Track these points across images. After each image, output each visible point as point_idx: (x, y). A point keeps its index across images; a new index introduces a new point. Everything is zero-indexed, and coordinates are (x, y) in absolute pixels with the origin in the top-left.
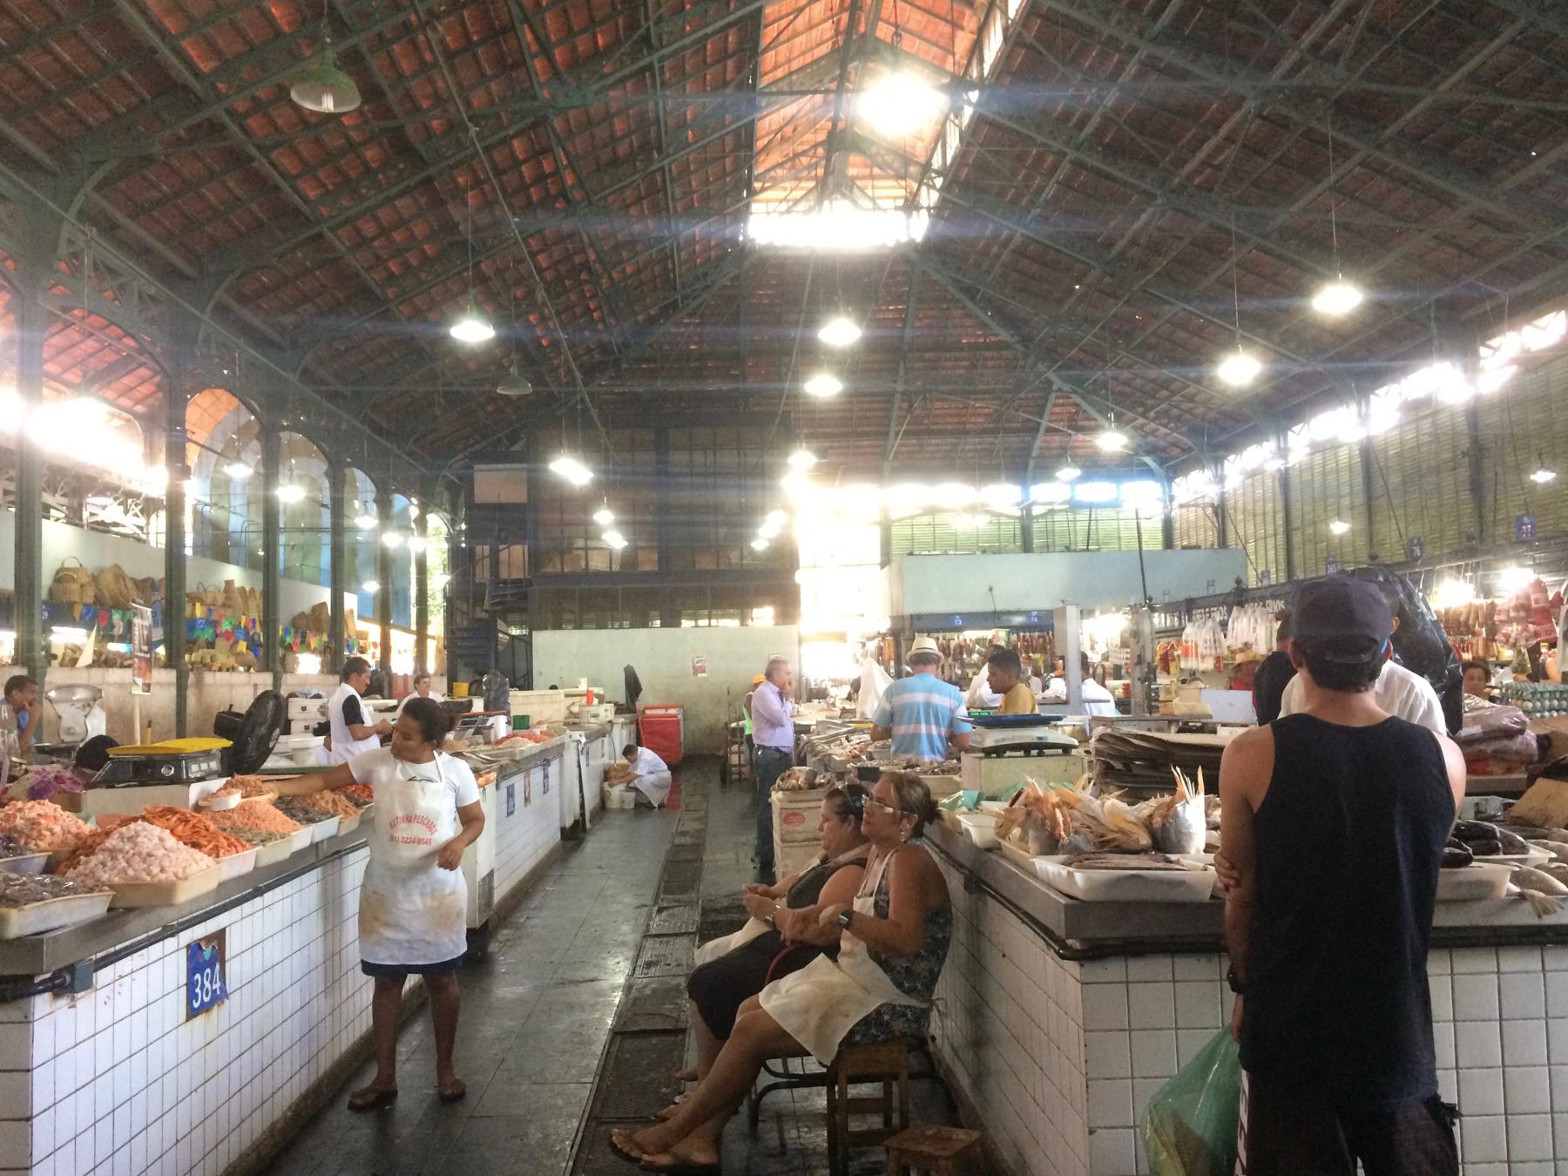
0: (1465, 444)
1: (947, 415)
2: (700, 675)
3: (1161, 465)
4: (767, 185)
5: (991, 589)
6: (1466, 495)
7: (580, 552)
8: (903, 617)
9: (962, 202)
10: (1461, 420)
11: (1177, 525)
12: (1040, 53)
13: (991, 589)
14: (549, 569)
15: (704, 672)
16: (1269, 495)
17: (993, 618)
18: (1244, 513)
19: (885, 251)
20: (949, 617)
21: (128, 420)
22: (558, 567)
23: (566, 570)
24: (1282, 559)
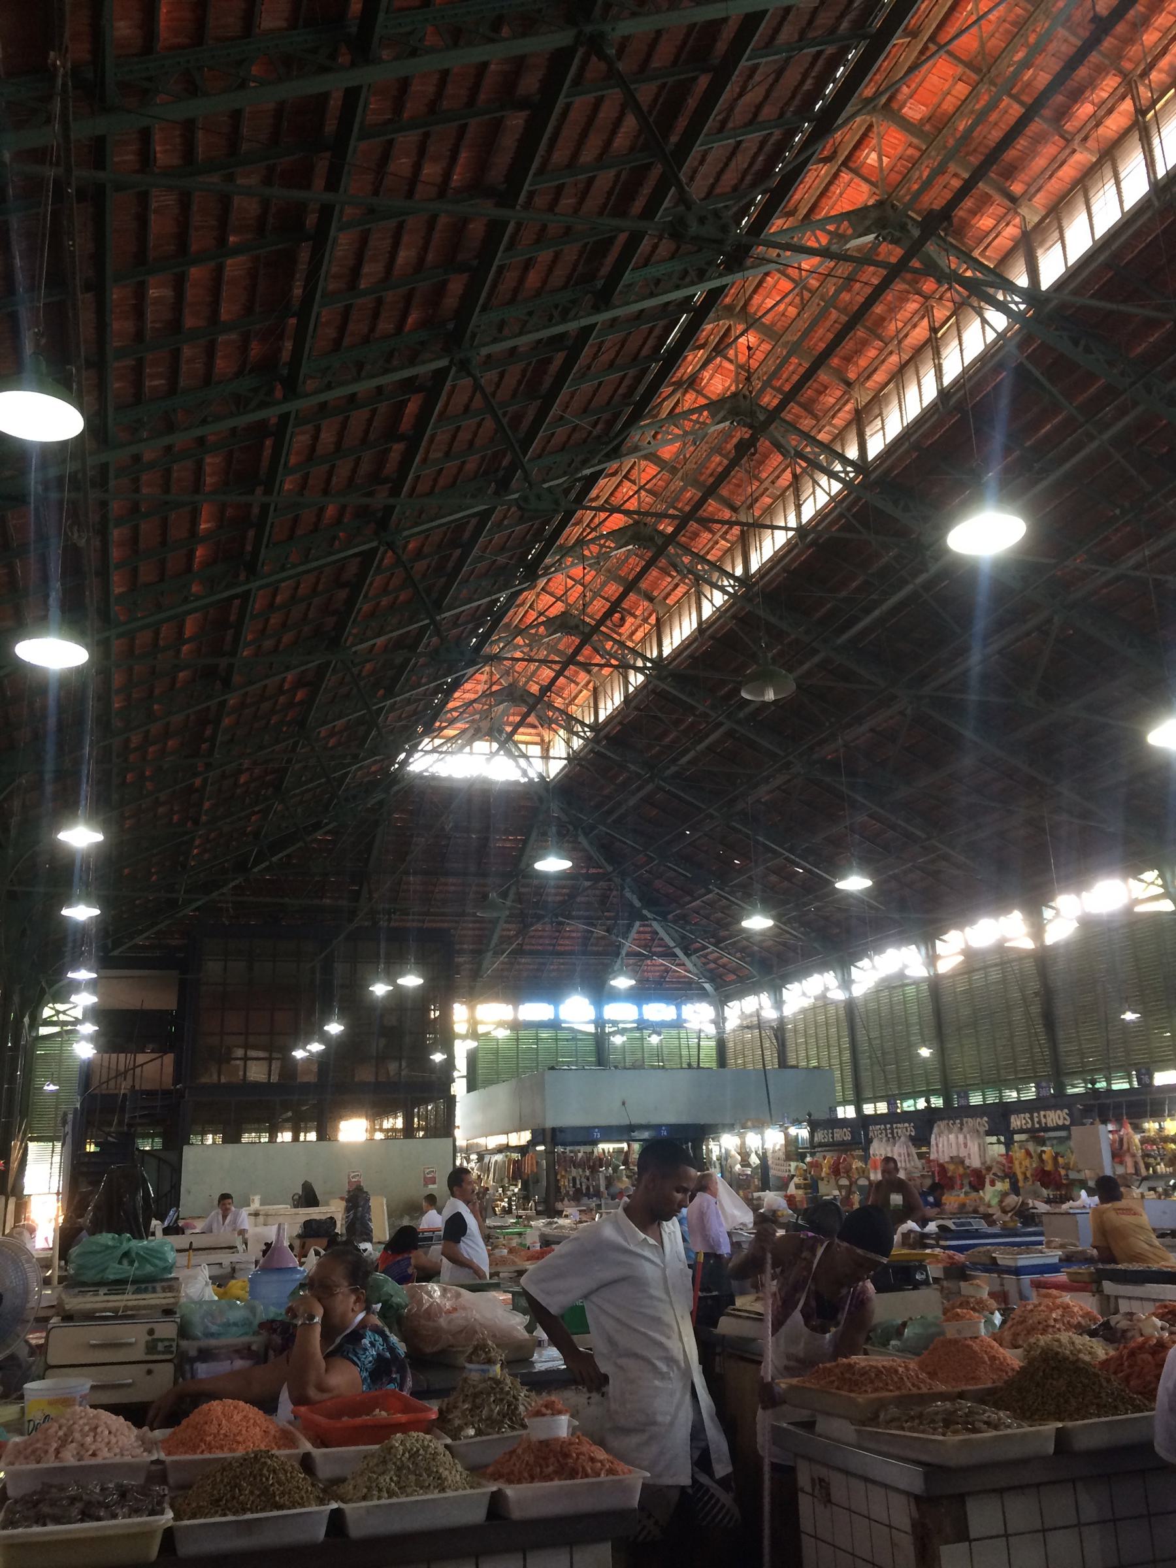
0: (1034, 985)
1: (541, 937)
2: (431, 1186)
3: (716, 990)
4: (444, 724)
5: (624, 1104)
6: (1040, 1029)
7: (238, 1062)
8: (544, 1130)
9: (609, 754)
10: (1029, 965)
11: (731, 1044)
12: (37, 509)
13: (624, 1104)
14: (204, 1080)
15: (434, 1183)
16: (832, 1021)
17: (624, 1132)
18: (806, 1036)
19: (519, 788)
20: (589, 1129)
21: (635, 964)
22: (215, 1077)
23: (223, 1080)
24: (849, 1079)
